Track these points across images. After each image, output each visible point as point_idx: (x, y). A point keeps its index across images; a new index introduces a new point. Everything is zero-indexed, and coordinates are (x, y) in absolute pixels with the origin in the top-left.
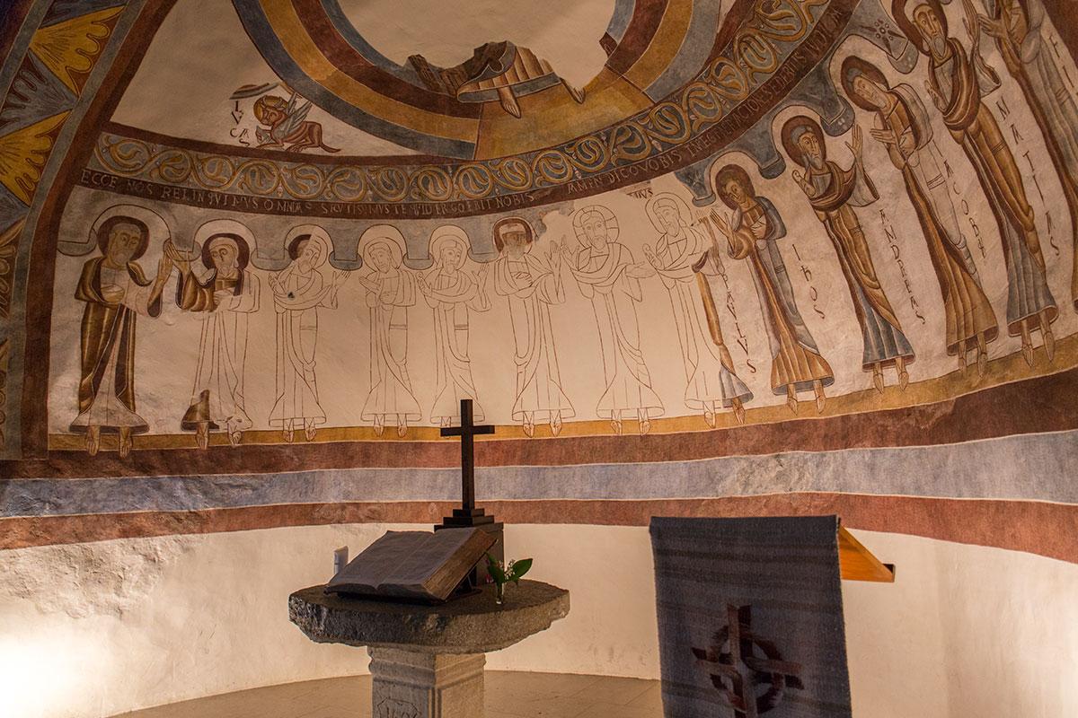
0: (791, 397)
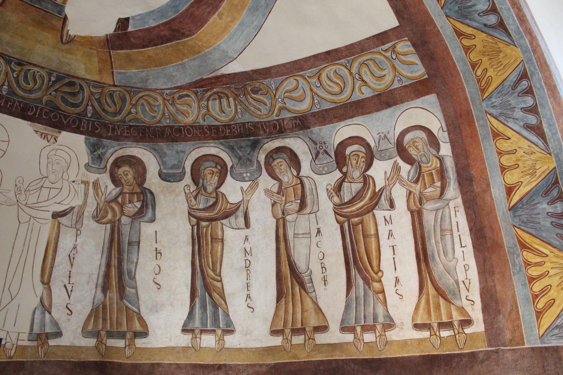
0: (100, 342)
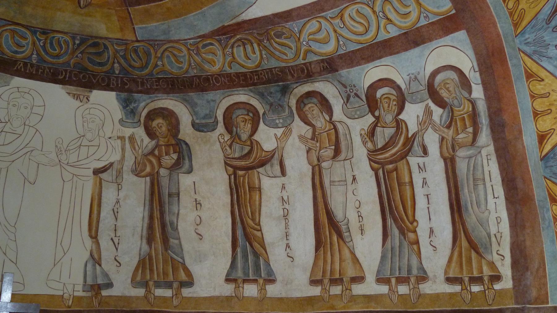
0: (148, 291)
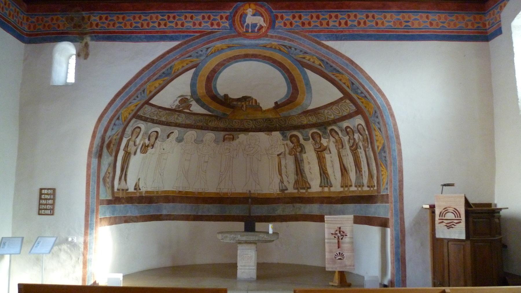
0: (298, 191)
